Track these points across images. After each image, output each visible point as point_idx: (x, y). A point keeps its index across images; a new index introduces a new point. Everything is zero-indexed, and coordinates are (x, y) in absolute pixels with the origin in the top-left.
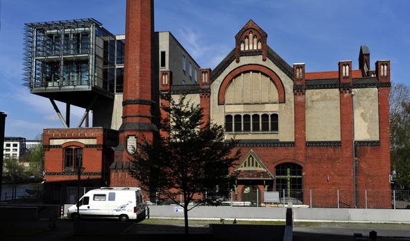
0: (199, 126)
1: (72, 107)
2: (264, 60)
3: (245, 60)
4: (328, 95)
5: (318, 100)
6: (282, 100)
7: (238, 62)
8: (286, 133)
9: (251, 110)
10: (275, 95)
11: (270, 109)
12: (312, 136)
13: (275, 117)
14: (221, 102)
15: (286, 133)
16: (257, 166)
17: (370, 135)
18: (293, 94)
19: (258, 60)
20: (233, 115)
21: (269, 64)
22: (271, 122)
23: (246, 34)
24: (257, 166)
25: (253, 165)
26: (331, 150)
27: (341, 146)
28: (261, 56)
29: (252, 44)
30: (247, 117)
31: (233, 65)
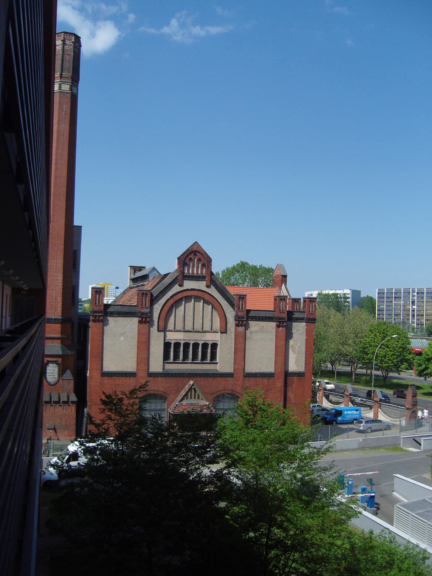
0: (274, 560)
1: (57, 33)
2: (208, 286)
3: (188, 284)
4: (265, 327)
5: (256, 332)
6: (224, 331)
7: (181, 285)
8: (224, 362)
9: (192, 338)
10: (217, 324)
11: (210, 338)
12: (250, 368)
13: (214, 346)
14: (163, 329)
15: (224, 362)
16: (198, 398)
17: (297, 366)
18: (389, 431)
19: (201, 285)
20: (173, 342)
21: (213, 291)
22: (209, 351)
23: (191, 256)
24: (198, 398)
25: (195, 398)
26: (265, 380)
27: (274, 377)
28: (205, 282)
29: (195, 269)
30: (187, 345)
31: (176, 288)
